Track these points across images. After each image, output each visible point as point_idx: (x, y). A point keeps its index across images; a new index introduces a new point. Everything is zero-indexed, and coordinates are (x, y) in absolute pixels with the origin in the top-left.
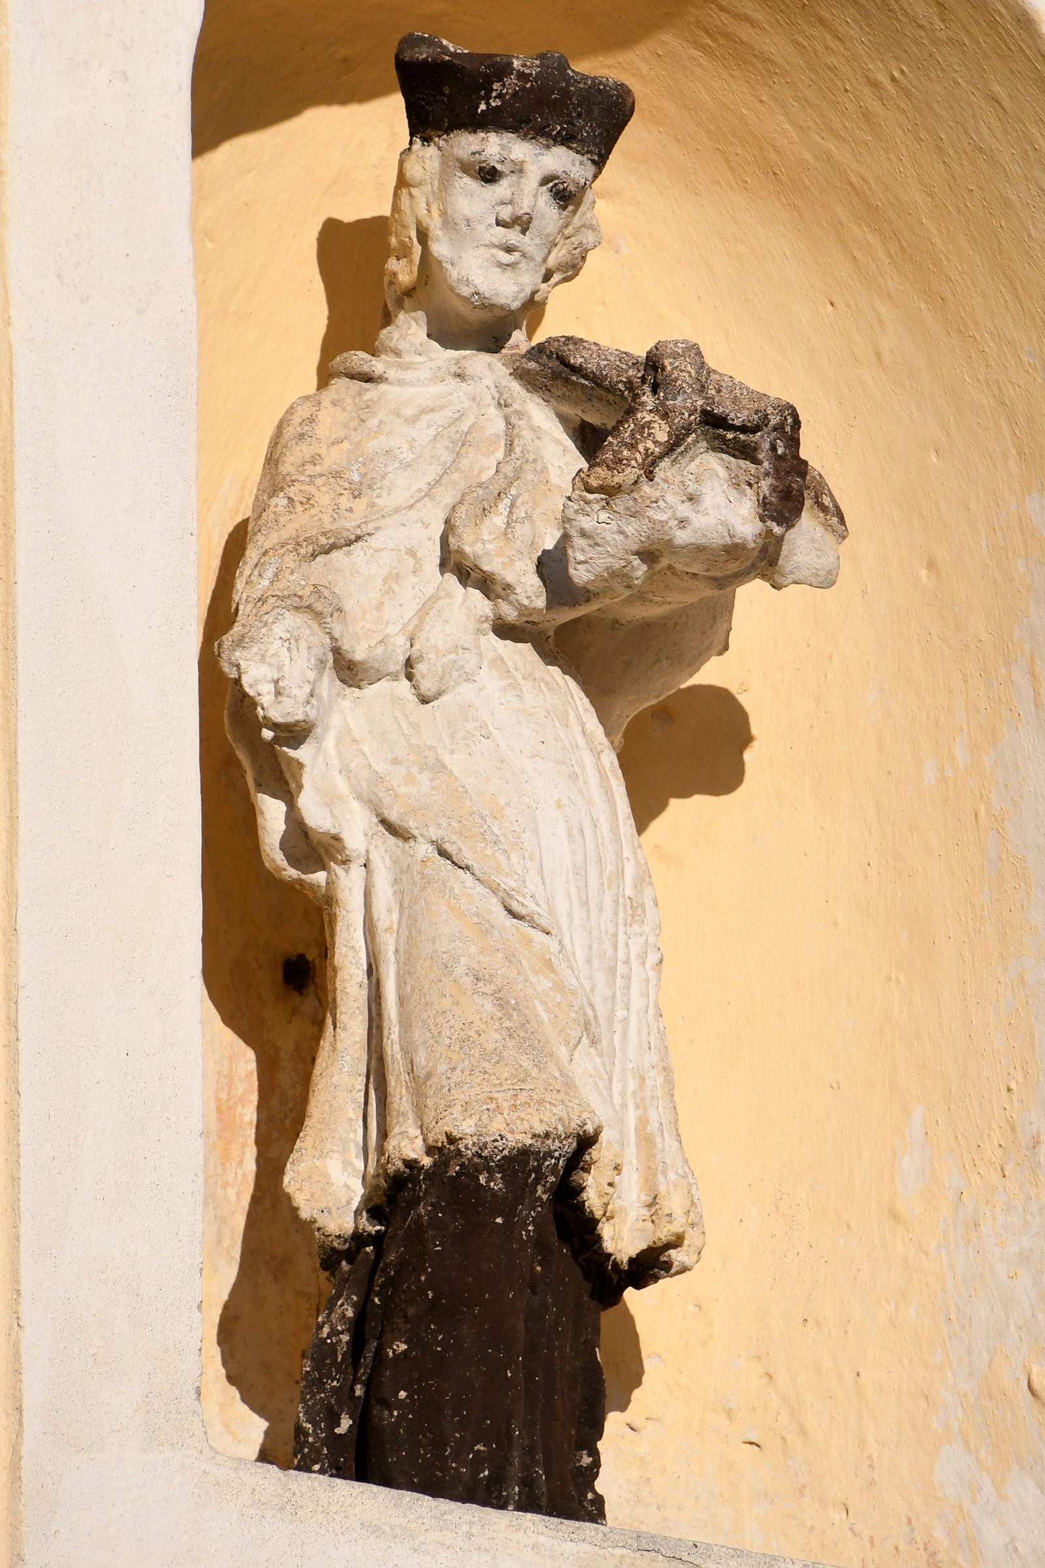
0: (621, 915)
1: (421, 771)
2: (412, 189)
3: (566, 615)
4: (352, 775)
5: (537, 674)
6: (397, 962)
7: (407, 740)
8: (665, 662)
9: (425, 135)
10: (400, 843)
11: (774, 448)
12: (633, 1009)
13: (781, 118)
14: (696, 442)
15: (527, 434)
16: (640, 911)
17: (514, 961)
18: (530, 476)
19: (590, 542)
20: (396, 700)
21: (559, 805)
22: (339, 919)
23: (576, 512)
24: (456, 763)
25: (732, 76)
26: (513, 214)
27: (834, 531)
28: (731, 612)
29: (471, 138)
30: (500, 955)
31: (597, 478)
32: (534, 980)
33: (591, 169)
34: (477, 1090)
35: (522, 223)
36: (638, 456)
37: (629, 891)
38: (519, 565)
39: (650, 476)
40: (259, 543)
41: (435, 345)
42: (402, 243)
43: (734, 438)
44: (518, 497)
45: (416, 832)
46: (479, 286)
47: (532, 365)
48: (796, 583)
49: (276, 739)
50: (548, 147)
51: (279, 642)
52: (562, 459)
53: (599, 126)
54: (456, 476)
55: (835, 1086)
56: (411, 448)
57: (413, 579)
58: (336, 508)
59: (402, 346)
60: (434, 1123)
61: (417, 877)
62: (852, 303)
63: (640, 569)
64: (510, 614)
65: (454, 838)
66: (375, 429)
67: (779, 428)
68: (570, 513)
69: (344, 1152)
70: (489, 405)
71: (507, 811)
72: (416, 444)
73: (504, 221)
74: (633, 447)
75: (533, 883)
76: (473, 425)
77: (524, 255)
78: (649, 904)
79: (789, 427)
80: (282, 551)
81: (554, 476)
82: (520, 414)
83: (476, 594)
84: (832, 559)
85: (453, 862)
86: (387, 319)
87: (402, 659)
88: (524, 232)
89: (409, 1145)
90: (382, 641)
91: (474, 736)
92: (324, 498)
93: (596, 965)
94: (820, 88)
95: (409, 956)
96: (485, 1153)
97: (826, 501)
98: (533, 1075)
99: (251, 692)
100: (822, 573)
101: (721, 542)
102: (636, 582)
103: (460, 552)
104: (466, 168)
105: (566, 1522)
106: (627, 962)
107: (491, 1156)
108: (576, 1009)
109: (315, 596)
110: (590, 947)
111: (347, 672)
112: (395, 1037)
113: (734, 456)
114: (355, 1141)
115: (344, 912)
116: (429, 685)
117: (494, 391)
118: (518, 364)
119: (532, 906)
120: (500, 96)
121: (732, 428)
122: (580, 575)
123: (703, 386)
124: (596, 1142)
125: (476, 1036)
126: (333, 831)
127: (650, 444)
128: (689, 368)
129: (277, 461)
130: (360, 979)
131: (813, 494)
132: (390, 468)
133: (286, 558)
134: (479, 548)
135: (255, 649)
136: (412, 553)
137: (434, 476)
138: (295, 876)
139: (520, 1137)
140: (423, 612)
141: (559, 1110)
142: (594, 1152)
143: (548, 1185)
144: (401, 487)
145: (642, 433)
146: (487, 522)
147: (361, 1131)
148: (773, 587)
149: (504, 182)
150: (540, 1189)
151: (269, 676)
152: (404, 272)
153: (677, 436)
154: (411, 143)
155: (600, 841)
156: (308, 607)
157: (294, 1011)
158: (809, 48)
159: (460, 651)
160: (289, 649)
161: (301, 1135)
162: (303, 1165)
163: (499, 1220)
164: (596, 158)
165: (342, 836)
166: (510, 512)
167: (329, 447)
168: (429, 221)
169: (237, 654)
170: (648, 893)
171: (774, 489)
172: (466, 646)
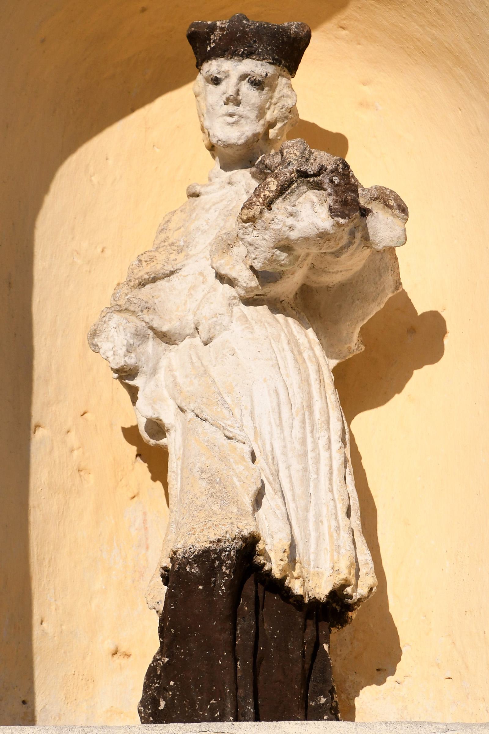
11: (331, 181)
13: (414, 23)
21: (265, 380)
23: (243, 234)
25: (389, 9)
27: (398, 217)
30: (216, 459)
31: (245, 215)
32: (235, 467)
38: (238, 268)
41: (222, 171)
50: (240, 61)
51: (114, 330)
67: (335, 171)
72: (209, 221)
83: (227, 286)
87: (193, 326)
100: (395, 239)
101: (314, 233)
105: (158, 725)
108: (255, 477)
109: (129, 303)
111: (165, 338)
113: (318, 190)
120: (214, 41)
128: (295, 152)
131: (382, 201)
135: (103, 336)
136: (201, 274)
138: (154, 443)
139: (203, 544)
143: (228, 565)
149: (224, 83)
150: (224, 568)
156: (126, 309)
159: (218, 316)
163: (200, 587)
165: (161, 418)
169: (96, 340)
171: (336, 201)
172: (221, 313)
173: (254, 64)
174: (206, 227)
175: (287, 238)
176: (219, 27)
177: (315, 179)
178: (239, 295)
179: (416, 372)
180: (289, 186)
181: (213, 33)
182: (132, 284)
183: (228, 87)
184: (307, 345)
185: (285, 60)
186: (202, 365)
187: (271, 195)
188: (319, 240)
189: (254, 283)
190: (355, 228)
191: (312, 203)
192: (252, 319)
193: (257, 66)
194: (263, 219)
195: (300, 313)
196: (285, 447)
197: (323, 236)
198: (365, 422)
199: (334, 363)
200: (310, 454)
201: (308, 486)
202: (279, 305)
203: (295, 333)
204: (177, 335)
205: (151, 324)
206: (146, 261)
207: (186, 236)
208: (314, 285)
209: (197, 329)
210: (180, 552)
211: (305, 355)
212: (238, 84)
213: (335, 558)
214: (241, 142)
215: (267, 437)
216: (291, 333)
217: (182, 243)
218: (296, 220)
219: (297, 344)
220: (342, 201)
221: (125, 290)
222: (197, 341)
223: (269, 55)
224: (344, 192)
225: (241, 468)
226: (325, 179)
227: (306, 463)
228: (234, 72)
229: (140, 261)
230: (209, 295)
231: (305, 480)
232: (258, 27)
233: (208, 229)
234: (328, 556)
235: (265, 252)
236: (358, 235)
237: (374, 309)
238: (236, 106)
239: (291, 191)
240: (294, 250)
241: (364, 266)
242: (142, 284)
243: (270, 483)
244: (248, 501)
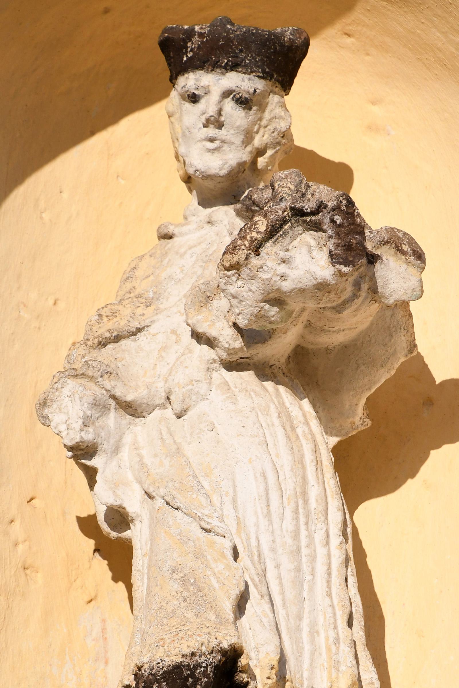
8: (363, 367)
11: (333, 221)
13: (434, 30)
21: (250, 461)
23: (225, 284)
24: (188, 450)
25: (405, 12)
27: (413, 265)
30: (190, 555)
32: (213, 566)
38: (218, 325)
39: (257, 253)
41: (200, 208)
43: (310, 220)
50: (223, 74)
51: (67, 398)
56: (182, 271)
66: (166, 265)
67: (337, 209)
72: (184, 268)
83: (205, 347)
87: (164, 395)
91: (204, 431)
93: (280, 551)
96: (154, 672)
100: (409, 292)
101: (311, 284)
108: (237, 578)
109: (86, 367)
113: (316, 231)
128: (289, 185)
131: (394, 245)
135: (55, 406)
138: (116, 536)
139: (174, 658)
149: (203, 101)
156: (83, 374)
159: (194, 383)
169: (46, 411)
171: (338, 245)
172: (198, 379)
173: (240, 78)
174: (180, 276)
175: (278, 289)
176: (198, 32)
177: (313, 218)
178: (219, 358)
179: (433, 453)
180: (281, 227)
181: (190, 40)
182: (90, 343)
183: (209, 105)
184: (302, 419)
185: (279, 75)
186: (175, 442)
187: (259, 237)
188: (317, 292)
189: (238, 343)
190: (361, 278)
191: (309, 247)
192: (236, 387)
193: (243, 80)
195: (293, 381)
196: (274, 541)
197: (322, 287)
198: (372, 514)
199: (334, 441)
200: (304, 551)
201: (301, 589)
202: (268, 371)
203: (288, 405)
204: (144, 405)
205: (113, 392)
206: (107, 316)
207: (156, 287)
208: (311, 347)
209: (168, 398)
210: (146, 667)
211: (299, 431)
212: (220, 102)
213: (334, 676)
214: (223, 172)
215: (252, 530)
216: (283, 404)
217: (151, 295)
218: (289, 268)
219: (289, 417)
220: (345, 246)
221: (82, 350)
222: (169, 413)
223: (258, 67)
224: (347, 234)
225: (221, 566)
226: (325, 218)
227: (300, 561)
228: (216, 88)
229: (100, 315)
230: (183, 358)
231: (298, 582)
232: (245, 33)
233: (183, 278)
234: (325, 674)
235: (251, 306)
236: (365, 286)
237: (383, 376)
238: (218, 129)
239: (284, 233)
240: (286, 304)
241: (372, 324)
242: (102, 344)
243: (255, 585)
244: (228, 607)
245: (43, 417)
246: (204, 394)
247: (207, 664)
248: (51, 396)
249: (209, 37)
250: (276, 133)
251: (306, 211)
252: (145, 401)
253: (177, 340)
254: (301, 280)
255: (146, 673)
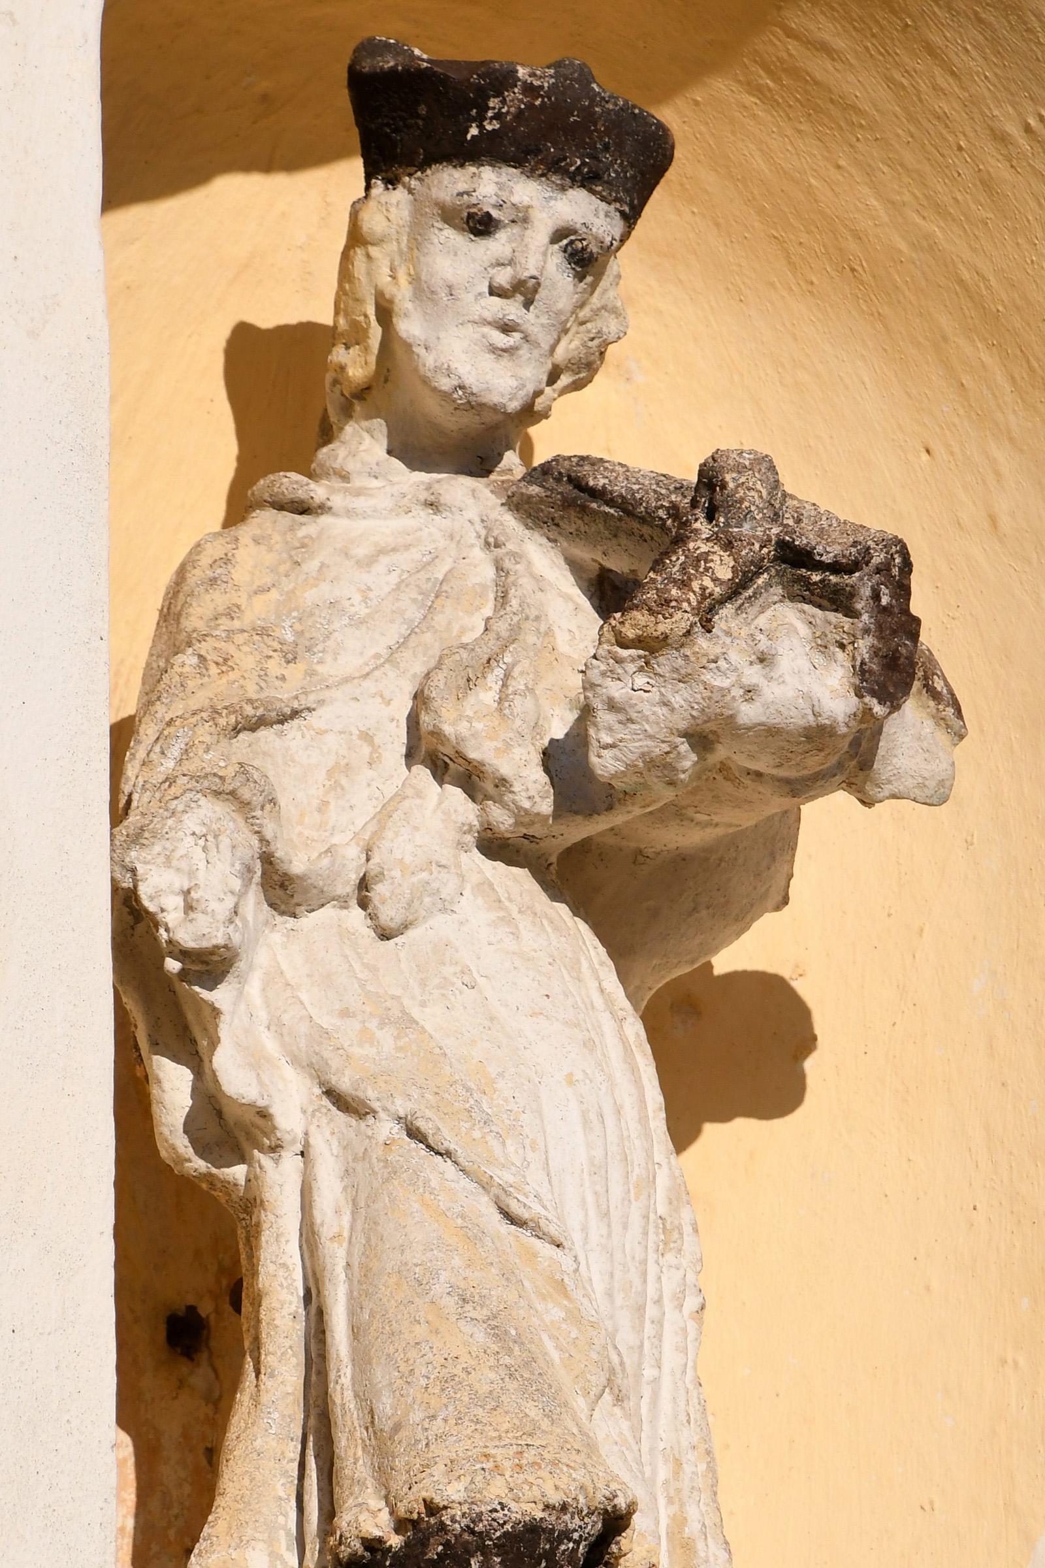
0: (652, 1237)
1: (382, 1025)
2: (371, 249)
3: (579, 830)
4: (285, 1031)
5: (538, 908)
6: (349, 1279)
7: (362, 986)
8: (704, 913)
9: (390, 175)
10: (353, 1121)
11: (876, 596)
12: (667, 1367)
13: (866, 190)
14: (768, 585)
15: (526, 583)
16: (675, 1235)
17: (514, 1279)
18: (531, 639)
19: (621, 717)
20: (345, 935)
21: (570, 1080)
22: (265, 1226)
23: (603, 674)
24: (430, 1018)
25: (799, 131)
26: (514, 277)
27: (948, 726)
28: (794, 849)
29: (457, 173)
31: (634, 626)
32: (540, 1307)
33: (616, 227)
34: (468, 1444)
35: (525, 291)
36: (692, 596)
37: (662, 1210)
38: (518, 753)
40: (159, 715)
41: (396, 463)
42: (355, 325)
44: (514, 665)
45: (376, 1105)
46: (465, 378)
47: (534, 490)
48: (894, 796)
49: (183, 975)
50: (563, 189)
52: (572, 620)
53: (632, 165)
54: (428, 637)
55: (927, 1507)
56: (365, 599)
57: (370, 773)
58: (264, 674)
59: (351, 466)
60: (405, 1489)
61: (378, 1166)
62: (956, 449)
63: (688, 760)
64: (503, 820)
65: (429, 1114)
66: (314, 574)
68: (594, 675)
69: (271, 1541)
70: (472, 546)
71: (501, 1084)
72: (371, 595)
73: (501, 288)
74: (684, 584)
75: (535, 1178)
76: (450, 571)
77: (526, 338)
78: (687, 1229)
79: (897, 570)
80: (193, 720)
81: (562, 642)
82: (516, 556)
83: (455, 793)
84: (944, 765)
85: (428, 1146)
86: (327, 434)
87: (354, 878)
88: (527, 304)
89: (369, 1518)
90: (328, 851)
91: (453, 984)
92: (246, 660)
93: (619, 1301)
94: (923, 146)
95: (366, 1271)
96: (480, 1527)
97: (939, 685)
98: (544, 1427)
99: (151, 907)
100: (932, 784)
101: (802, 722)
102: (682, 776)
103: (437, 734)
104: (448, 215)
106: (659, 1301)
107: (488, 1532)
110: (612, 1276)
111: (280, 892)
112: (346, 1380)
113: (820, 607)
114: (284, 1527)
115: (271, 1217)
116: (392, 913)
117: (479, 527)
118: (514, 488)
119: (537, 1208)
121: (820, 566)
122: (605, 764)
123: (776, 514)
124: (626, 1527)
125: (464, 1375)
126: (261, 1103)
127: (707, 582)
128: (759, 486)
129: (179, 615)
130: (293, 1308)
132: (336, 625)
133: (200, 730)
134: (463, 728)
135: (157, 848)
136: (367, 737)
137: (396, 637)
139: (528, 1507)
140: (384, 815)
141: (579, 1475)
142: (624, 1541)
144: (350, 651)
145: (696, 568)
146: (472, 698)
147: (293, 1515)
148: (863, 802)
149: (502, 236)
151: (177, 886)
152: (356, 364)
153: (744, 573)
154: (368, 188)
155: (625, 1133)
156: (232, 793)
157: (181, 1384)
158: (910, 89)
160: (205, 849)
161: (210, 1518)
162: (214, 1557)
164: (627, 209)
165: (272, 1111)
166: (504, 685)
167: (250, 597)
168: (394, 290)
169: (133, 854)
170: (686, 1215)
171: (875, 652)
172: (443, 862)
173: (593, 207)
176: (525, 82)
194: (687, 651)
218: (765, 677)
228: (544, 215)
235: (651, 737)
239: (755, 593)
245: (124, 867)
246: (448, 898)
247: (581, 1536)
248: (156, 824)
249: (550, 99)
250: (596, 342)
251: (818, 558)
252: (321, 883)
253: (371, 757)
254: (782, 709)
255: (457, 1526)
